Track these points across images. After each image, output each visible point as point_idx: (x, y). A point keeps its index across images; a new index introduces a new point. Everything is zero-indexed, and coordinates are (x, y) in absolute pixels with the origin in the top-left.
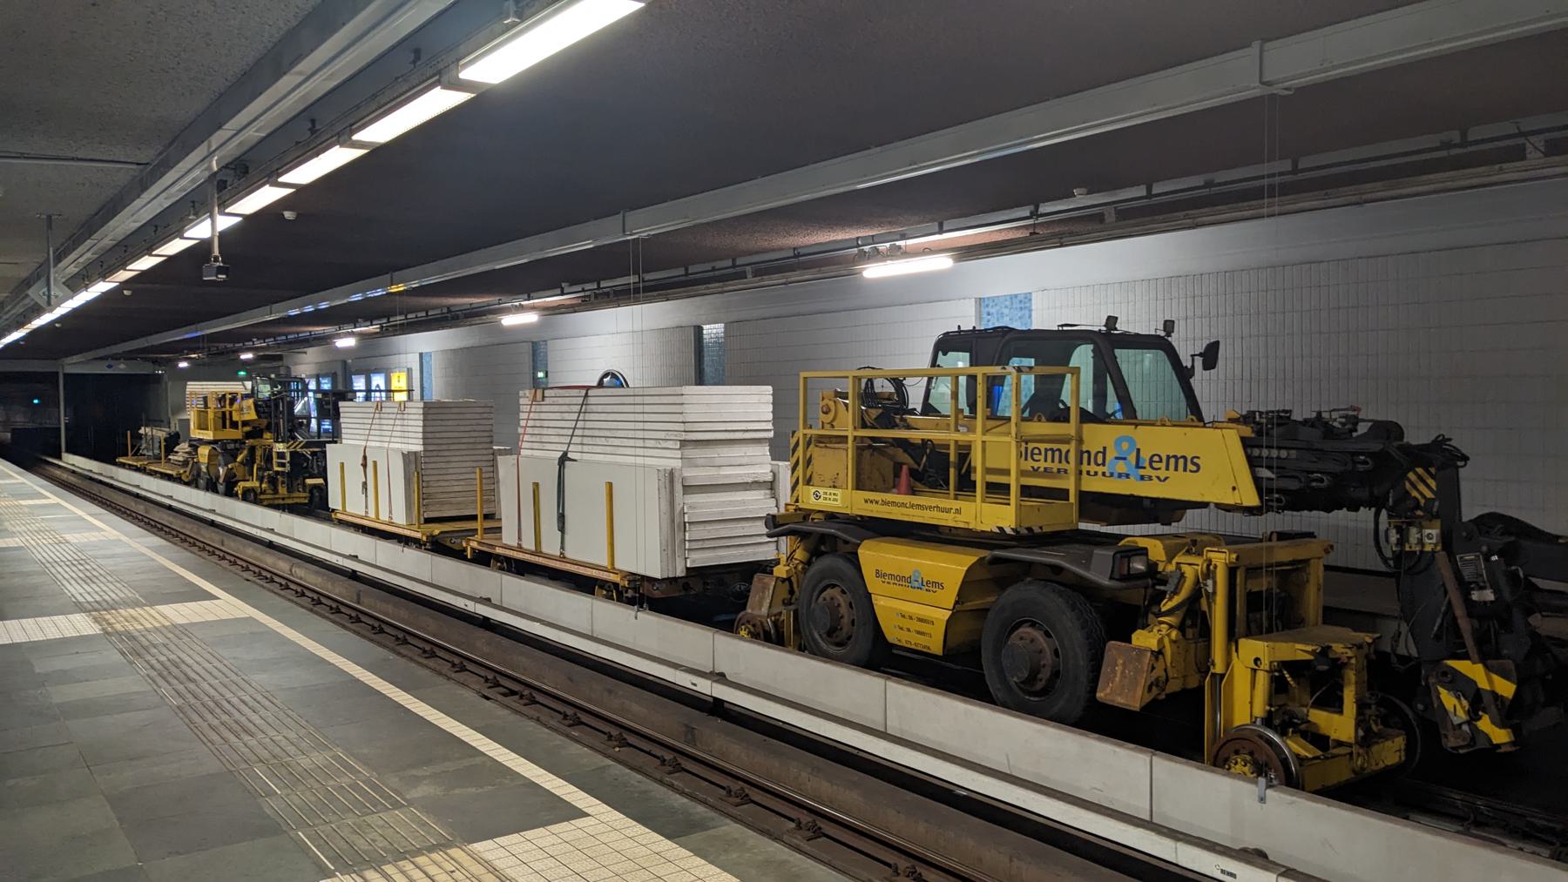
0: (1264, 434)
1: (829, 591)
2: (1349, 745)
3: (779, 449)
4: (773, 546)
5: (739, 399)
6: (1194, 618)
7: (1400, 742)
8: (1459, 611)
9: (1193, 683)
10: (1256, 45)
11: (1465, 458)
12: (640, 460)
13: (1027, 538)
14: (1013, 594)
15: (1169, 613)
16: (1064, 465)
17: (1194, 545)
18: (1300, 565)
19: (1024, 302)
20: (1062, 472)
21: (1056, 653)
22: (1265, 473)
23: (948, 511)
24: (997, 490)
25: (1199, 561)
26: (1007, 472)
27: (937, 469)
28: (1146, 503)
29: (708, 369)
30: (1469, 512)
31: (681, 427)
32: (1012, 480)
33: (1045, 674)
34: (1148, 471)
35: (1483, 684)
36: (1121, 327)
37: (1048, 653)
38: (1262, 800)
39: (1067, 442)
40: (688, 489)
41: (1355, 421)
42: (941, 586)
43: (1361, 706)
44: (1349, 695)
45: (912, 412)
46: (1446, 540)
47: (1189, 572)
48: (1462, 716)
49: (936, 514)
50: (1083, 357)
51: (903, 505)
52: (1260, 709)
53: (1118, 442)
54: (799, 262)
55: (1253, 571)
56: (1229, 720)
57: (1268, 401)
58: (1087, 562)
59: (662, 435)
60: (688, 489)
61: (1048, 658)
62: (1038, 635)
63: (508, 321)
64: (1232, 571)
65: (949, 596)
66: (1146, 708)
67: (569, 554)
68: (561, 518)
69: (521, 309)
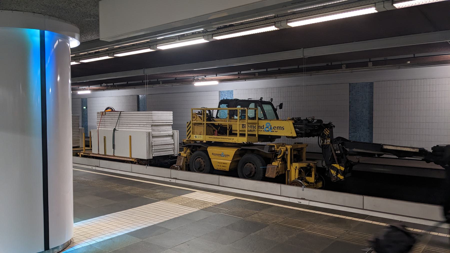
0: (297, 122)
1: (198, 159)
2: (313, 183)
3: (174, 127)
4: (173, 151)
5: (165, 115)
6: (284, 160)
7: (321, 183)
8: (334, 155)
9: (284, 173)
10: (302, 49)
11: (334, 126)
12: (128, 130)
14: (246, 156)
15: (279, 158)
16: (254, 129)
17: (283, 145)
18: (302, 148)
19: (231, 92)
20: (254, 131)
21: (255, 168)
22: (297, 130)
23: (230, 139)
24: (243, 135)
25: (284, 148)
26: (237, 131)
27: (223, 130)
28: (270, 137)
29: (141, 107)
30: (335, 137)
31: (152, 121)
32: (238, 132)
33: (253, 173)
34: (273, 130)
35: (339, 168)
36: (263, 100)
37: (254, 168)
38: (303, 190)
39: (256, 124)
40: (153, 137)
41: (313, 119)
42: (229, 156)
43: (315, 175)
44: (313, 174)
45: (214, 118)
46: (331, 142)
47: (283, 150)
48: (335, 174)
49: (227, 140)
51: (219, 138)
52: (297, 177)
53: (266, 124)
54: (176, 81)
55: (294, 150)
56: (291, 180)
57: (297, 116)
58: (263, 149)
59: (145, 124)
60: (153, 137)
61: (254, 169)
62: (251, 165)
63: (80, 93)
64: (291, 149)
66: (276, 177)
67: (115, 155)
69: (87, 89)
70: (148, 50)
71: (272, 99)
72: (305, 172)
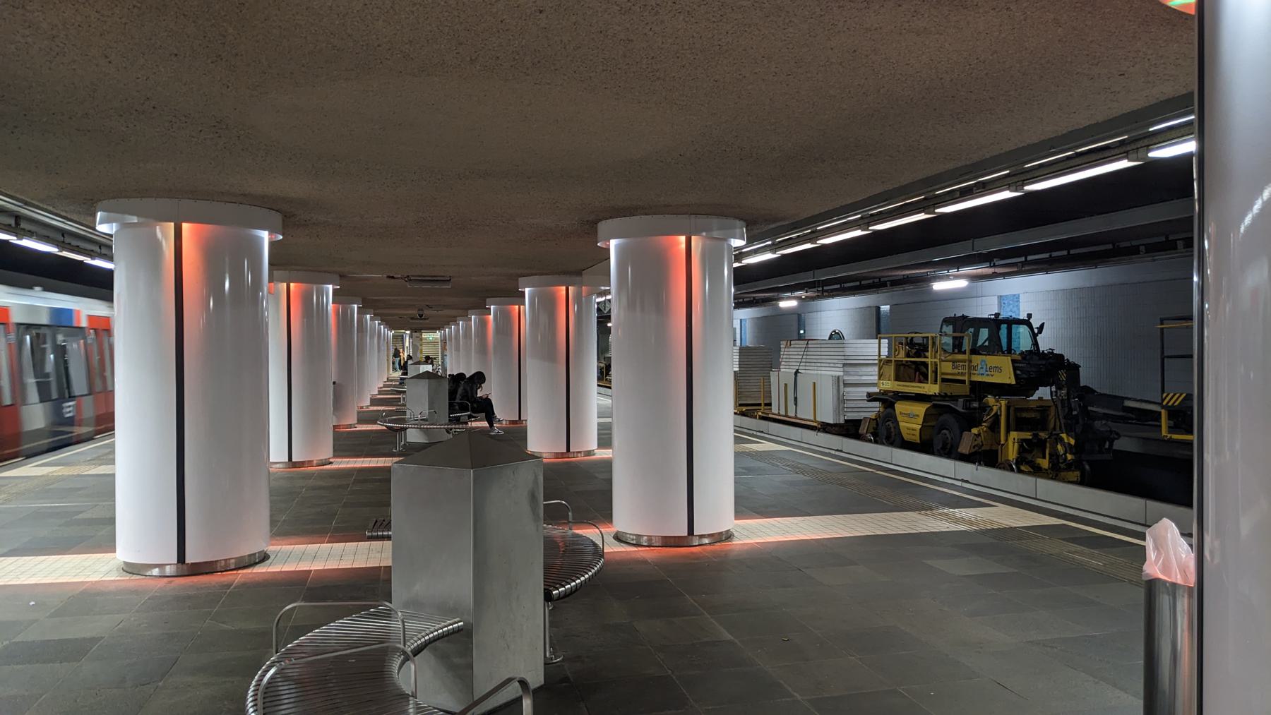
6: (994, 426)
13: (943, 396)
19: (1016, 298)
40: (846, 385)
50: (1004, 327)
60: (846, 385)
63: (938, 286)
65: (920, 420)
68: (796, 399)
70: (921, 216)
71: (1030, 316)
72: (1026, 450)
